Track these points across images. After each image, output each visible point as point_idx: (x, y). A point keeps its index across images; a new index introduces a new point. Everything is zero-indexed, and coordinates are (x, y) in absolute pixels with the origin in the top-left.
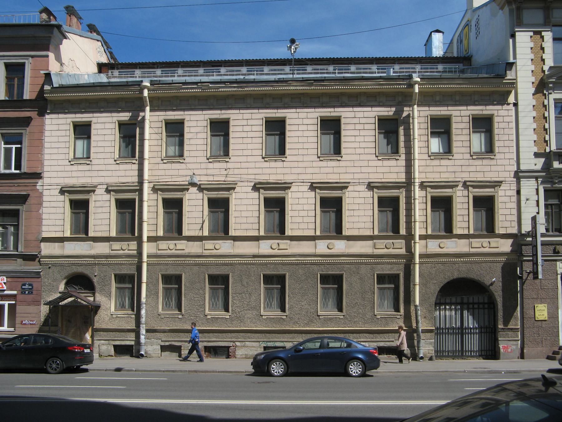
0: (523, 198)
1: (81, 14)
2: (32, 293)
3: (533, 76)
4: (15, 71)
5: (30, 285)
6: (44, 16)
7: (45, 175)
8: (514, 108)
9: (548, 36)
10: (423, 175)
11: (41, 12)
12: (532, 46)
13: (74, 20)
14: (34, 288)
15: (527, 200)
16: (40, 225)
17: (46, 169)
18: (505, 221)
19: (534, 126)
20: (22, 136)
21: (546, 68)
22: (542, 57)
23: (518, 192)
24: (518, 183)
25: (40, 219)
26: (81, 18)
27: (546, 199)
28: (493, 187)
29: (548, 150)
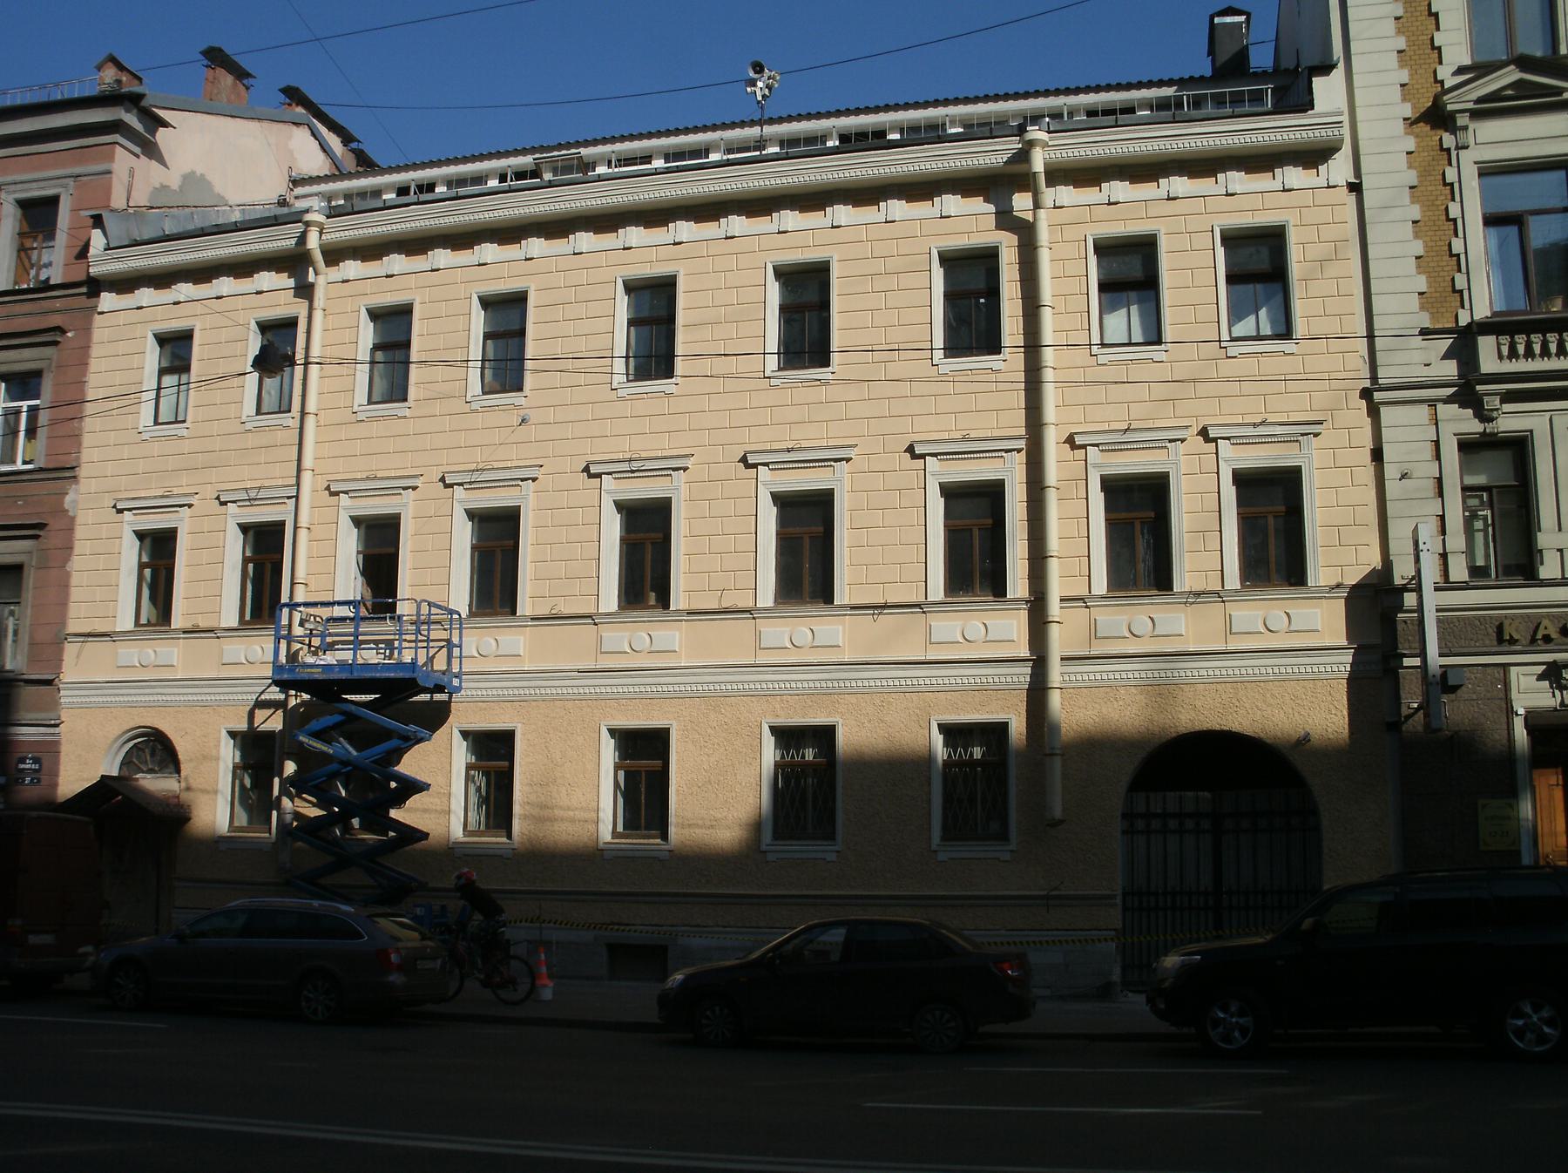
0: (1391, 472)
1: (244, 62)
2: (39, 781)
3: (1404, 100)
4: (38, 216)
5: (36, 760)
6: (110, 74)
7: (83, 472)
8: (1353, 197)
9: (1526, 860)
10: (1078, 415)
11: (99, 68)
12: (1400, 12)
13: (228, 79)
14: (44, 770)
15: (1404, 476)
16: (63, 603)
17: (86, 455)
18: (1339, 549)
19: (1418, 248)
20: (675, 284)
21: (1445, 73)
22: (1432, 39)
23: (1377, 455)
24: (1374, 411)
25: (64, 586)
26: (248, 75)
27: (1464, 468)
28: (1293, 440)
29: (1464, 319)
